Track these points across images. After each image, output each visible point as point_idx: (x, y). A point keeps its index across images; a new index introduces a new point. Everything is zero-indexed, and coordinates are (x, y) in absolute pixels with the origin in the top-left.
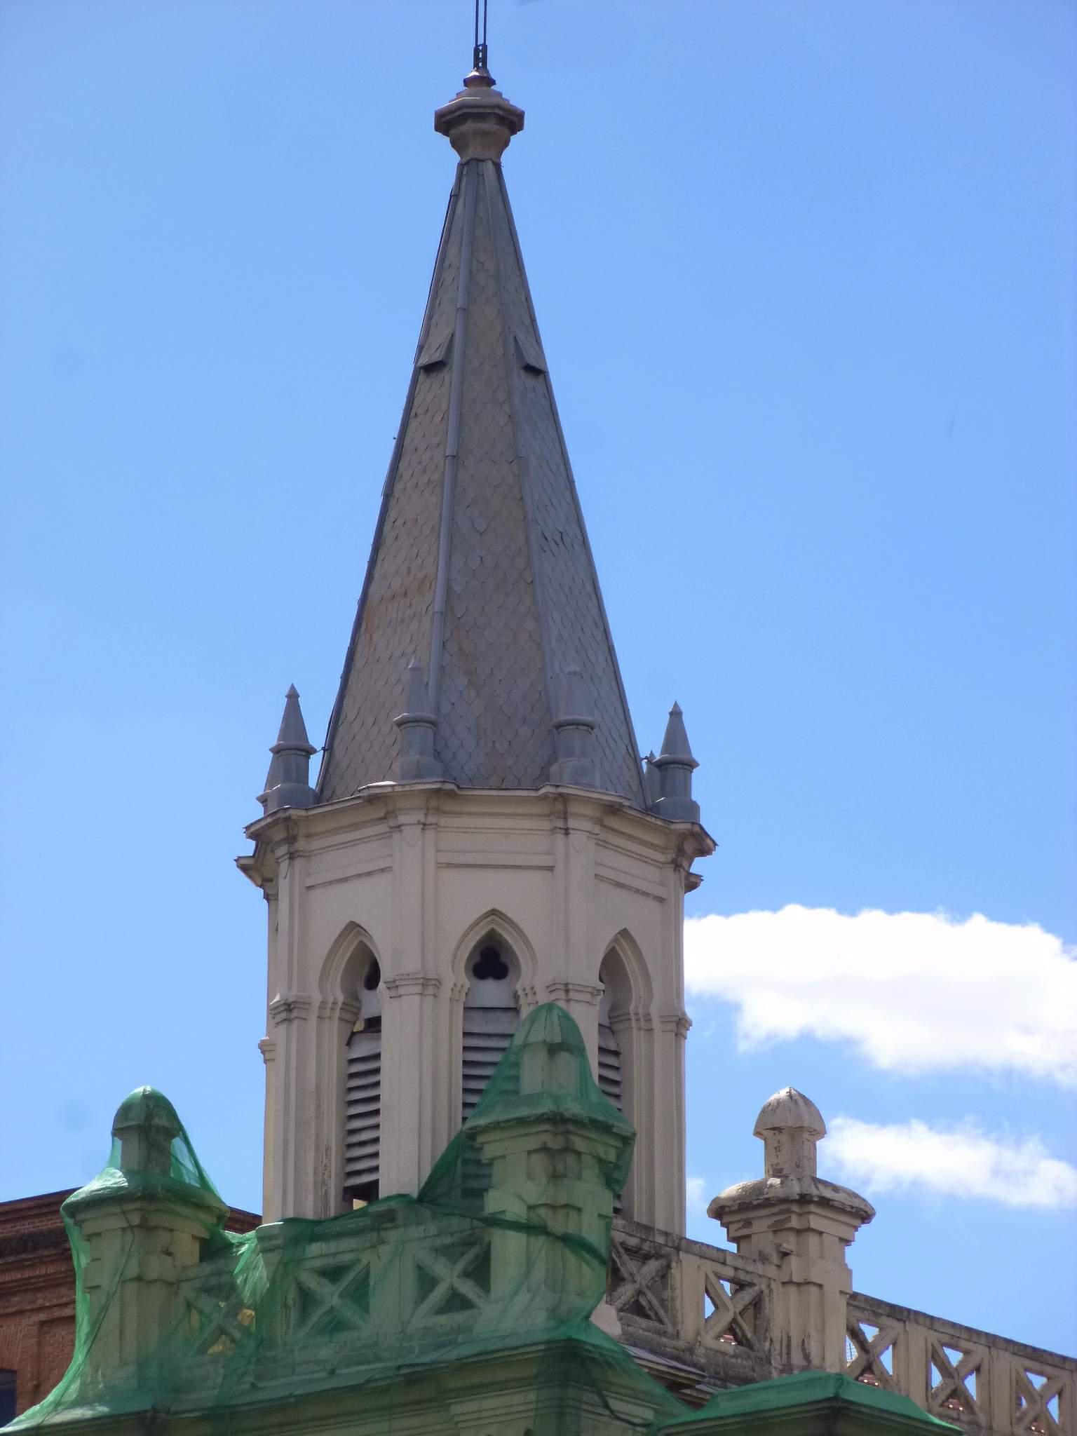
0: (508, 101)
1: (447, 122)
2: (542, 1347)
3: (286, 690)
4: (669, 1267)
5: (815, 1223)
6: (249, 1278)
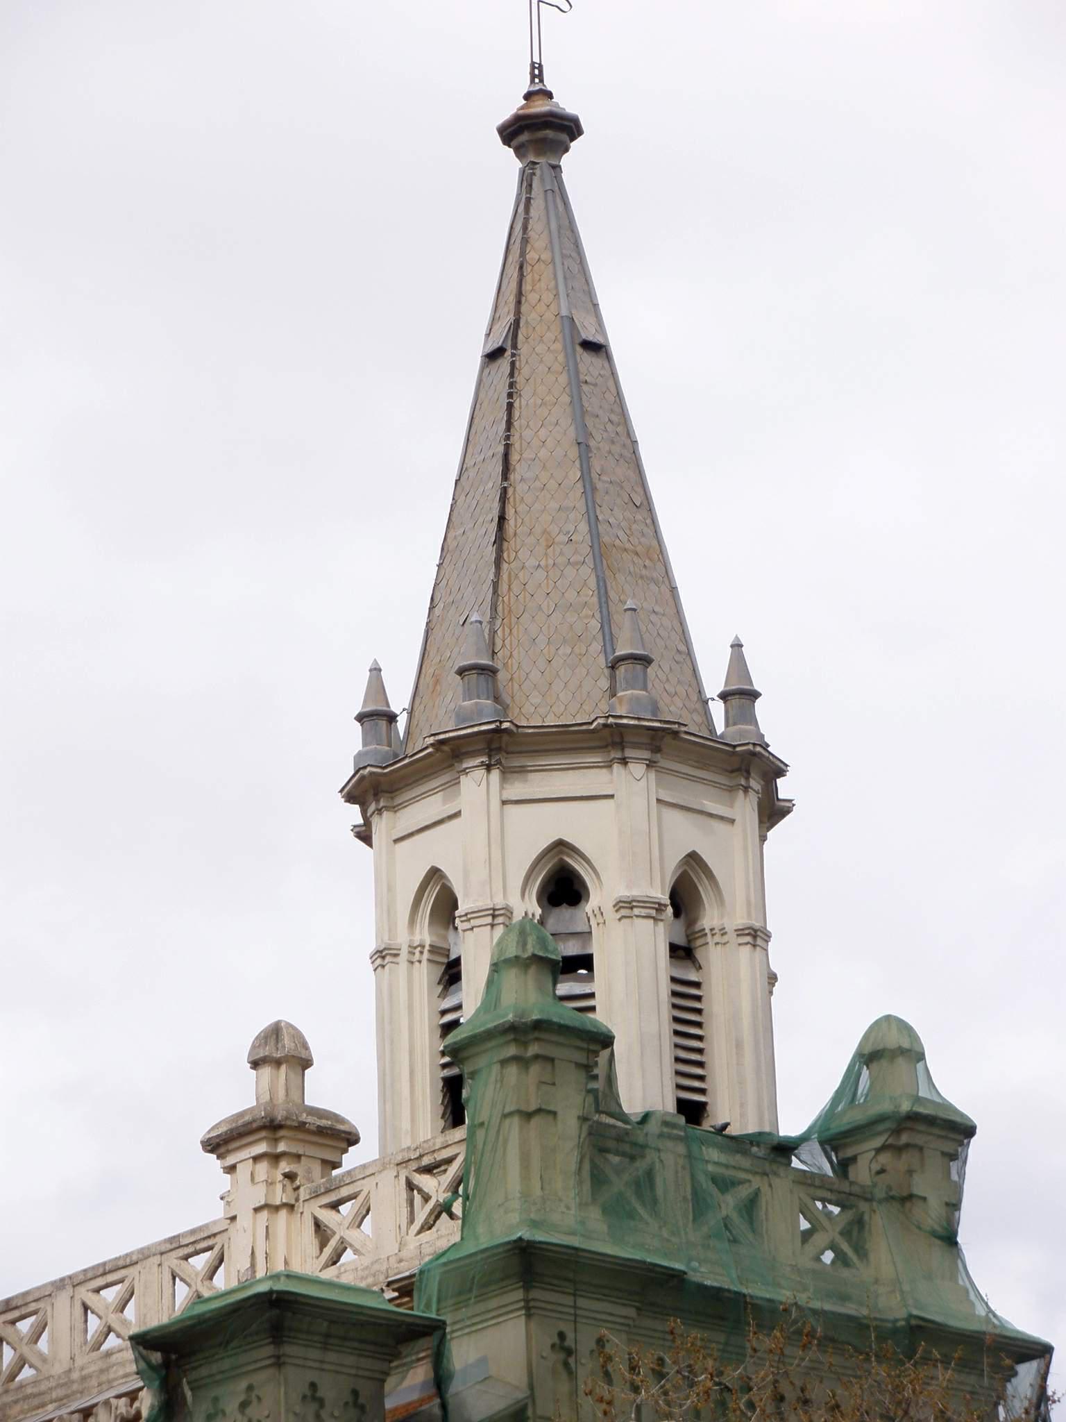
0: (564, 109)
1: (512, 132)
2: (501, 1250)
3: (369, 666)
5: (919, 1139)
6: (415, 709)
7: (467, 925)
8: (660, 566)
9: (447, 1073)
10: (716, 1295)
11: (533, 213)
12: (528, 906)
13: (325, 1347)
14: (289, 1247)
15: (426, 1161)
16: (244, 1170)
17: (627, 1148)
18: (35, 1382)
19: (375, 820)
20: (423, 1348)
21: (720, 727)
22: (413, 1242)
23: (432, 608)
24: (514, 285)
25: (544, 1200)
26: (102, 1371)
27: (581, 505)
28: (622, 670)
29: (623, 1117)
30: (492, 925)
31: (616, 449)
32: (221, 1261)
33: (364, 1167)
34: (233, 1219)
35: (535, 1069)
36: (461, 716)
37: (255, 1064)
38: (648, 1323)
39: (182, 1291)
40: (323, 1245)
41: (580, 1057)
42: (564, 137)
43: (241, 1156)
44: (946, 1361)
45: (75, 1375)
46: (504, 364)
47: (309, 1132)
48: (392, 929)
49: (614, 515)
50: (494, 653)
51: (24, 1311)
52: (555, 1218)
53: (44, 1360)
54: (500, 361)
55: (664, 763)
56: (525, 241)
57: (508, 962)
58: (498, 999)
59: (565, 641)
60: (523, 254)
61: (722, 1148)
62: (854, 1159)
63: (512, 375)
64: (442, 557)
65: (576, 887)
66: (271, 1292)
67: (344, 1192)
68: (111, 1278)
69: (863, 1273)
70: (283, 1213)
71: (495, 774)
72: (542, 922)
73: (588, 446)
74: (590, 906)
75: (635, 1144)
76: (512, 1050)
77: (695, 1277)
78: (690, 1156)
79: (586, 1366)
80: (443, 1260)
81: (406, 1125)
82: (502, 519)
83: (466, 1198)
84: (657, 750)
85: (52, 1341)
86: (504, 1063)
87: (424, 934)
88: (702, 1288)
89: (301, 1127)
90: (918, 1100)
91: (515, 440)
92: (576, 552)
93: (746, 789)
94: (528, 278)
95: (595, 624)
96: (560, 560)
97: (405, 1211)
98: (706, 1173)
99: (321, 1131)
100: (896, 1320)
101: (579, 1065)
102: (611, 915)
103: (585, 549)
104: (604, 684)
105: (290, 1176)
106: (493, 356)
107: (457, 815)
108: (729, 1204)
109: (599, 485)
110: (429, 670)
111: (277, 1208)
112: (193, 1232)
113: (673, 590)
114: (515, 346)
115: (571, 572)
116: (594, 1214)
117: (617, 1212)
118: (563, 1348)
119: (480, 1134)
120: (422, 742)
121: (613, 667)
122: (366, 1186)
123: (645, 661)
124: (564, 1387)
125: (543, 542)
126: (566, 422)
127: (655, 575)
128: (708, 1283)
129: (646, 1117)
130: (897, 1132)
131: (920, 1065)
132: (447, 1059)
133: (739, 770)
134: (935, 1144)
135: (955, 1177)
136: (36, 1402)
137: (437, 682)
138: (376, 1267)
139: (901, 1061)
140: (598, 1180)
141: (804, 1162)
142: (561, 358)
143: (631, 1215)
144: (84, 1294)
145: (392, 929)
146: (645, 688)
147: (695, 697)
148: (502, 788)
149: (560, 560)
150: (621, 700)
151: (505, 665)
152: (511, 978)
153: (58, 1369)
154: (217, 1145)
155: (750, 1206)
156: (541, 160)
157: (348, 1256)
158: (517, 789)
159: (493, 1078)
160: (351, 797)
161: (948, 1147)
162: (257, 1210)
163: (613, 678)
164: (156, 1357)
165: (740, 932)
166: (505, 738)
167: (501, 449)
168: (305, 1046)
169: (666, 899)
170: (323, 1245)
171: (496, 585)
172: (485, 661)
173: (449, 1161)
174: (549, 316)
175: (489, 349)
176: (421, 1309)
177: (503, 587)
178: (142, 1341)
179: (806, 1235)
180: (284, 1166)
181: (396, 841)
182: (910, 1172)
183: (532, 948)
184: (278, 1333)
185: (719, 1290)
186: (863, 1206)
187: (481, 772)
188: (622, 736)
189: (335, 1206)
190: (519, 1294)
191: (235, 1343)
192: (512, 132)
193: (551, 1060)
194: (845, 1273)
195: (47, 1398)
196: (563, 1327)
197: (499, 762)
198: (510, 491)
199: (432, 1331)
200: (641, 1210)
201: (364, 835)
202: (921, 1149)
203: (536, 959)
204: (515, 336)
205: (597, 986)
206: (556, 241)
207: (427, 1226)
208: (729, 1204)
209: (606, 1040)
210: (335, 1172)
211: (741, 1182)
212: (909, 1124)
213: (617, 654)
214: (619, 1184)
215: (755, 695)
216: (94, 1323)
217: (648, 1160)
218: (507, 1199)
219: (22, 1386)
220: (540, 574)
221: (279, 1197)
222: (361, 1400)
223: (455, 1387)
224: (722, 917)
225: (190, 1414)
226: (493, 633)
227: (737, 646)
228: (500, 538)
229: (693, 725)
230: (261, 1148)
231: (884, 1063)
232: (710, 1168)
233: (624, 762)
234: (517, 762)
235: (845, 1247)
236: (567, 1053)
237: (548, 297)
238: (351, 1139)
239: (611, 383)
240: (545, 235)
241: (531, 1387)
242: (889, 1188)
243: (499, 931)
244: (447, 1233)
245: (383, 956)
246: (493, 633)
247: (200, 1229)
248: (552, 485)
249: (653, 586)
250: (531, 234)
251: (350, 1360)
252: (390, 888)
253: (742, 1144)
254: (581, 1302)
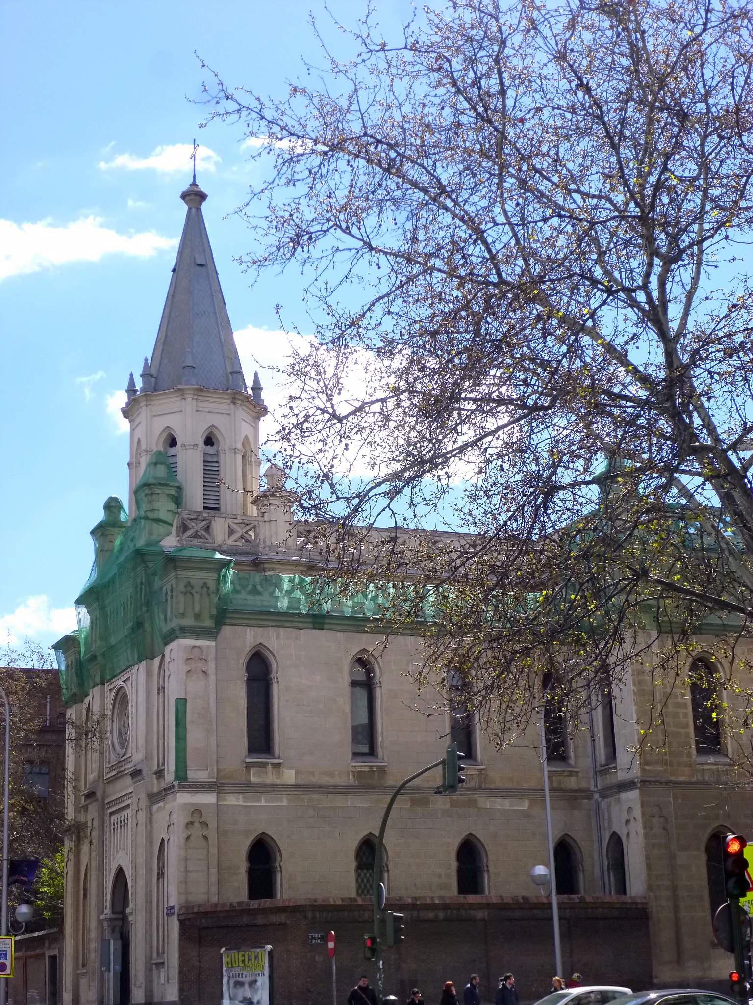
4: (210, 522)
192: (184, 196)
233: (185, 399)
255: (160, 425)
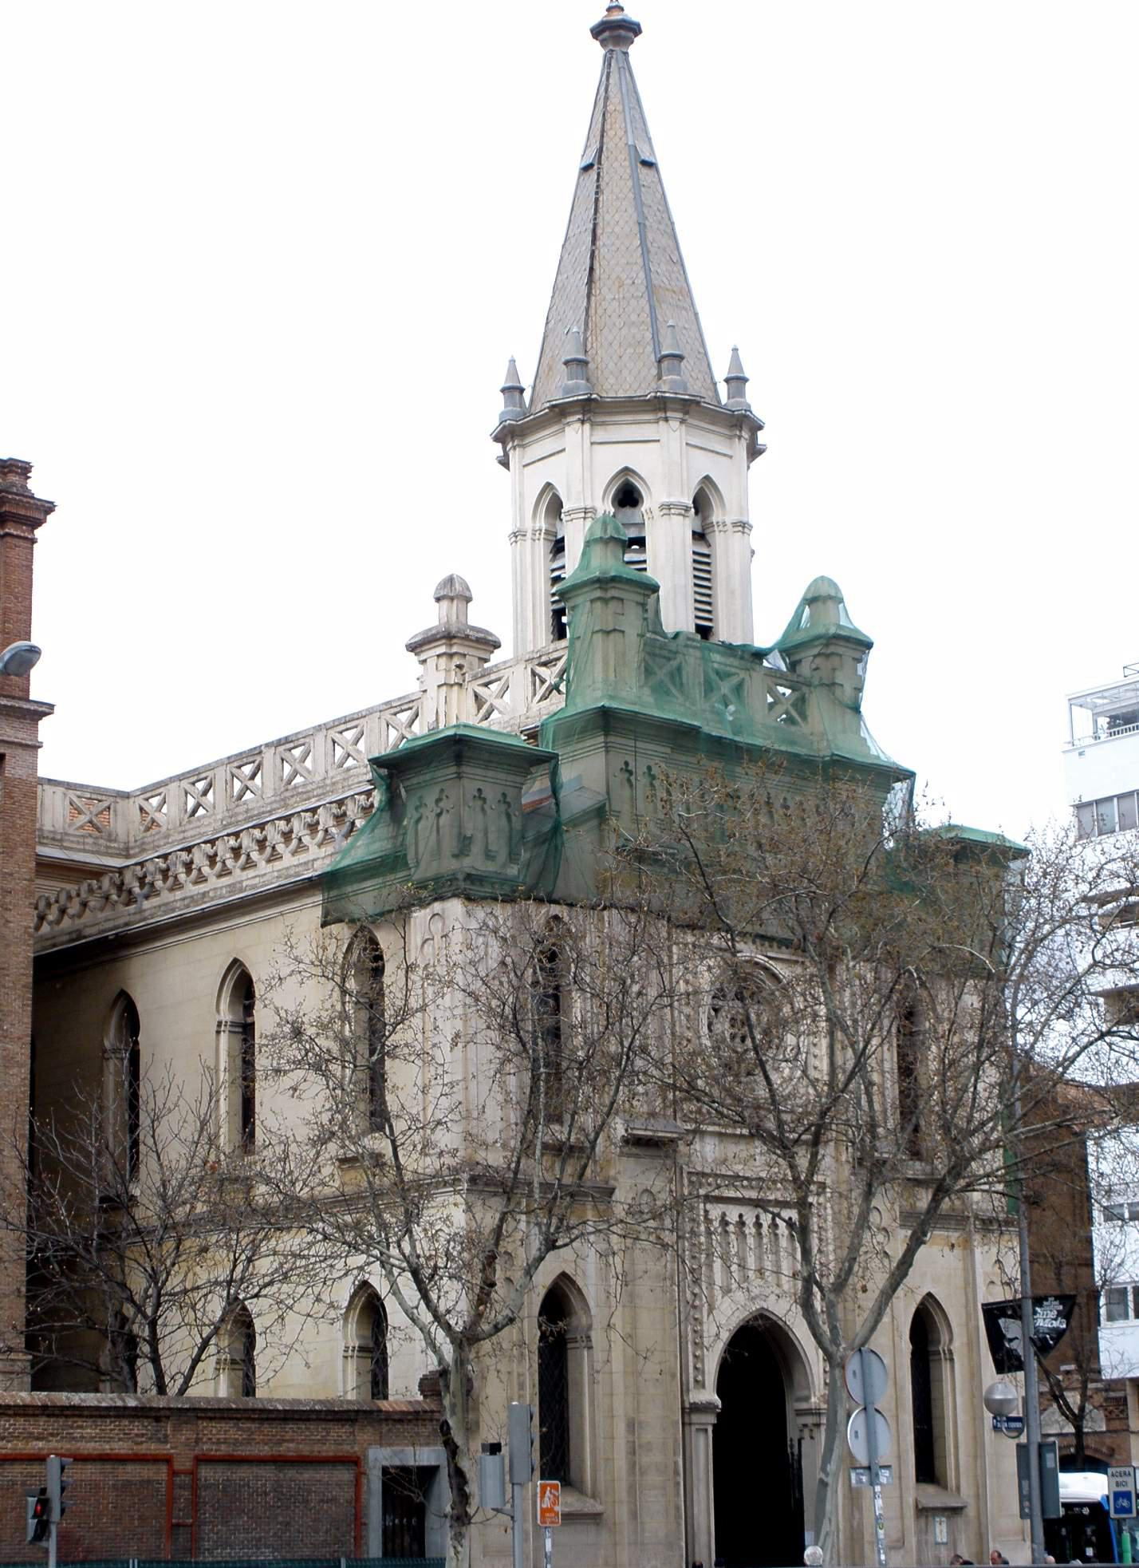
1: (598, 32)
5: (840, 650)
7: (569, 518)
8: (688, 300)
9: (555, 607)
10: (719, 741)
11: (611, 81)
12: (606, 507)
13: (487, 768)
14: (459, 709)
15: (543, 659)
16: (431, 663)
17: (665, 653)
18: (304, 785)
19: (511, 454)
20: (545, 769)
21: (724, 399)
22: (535, 706)
23: (547, 323)
24: (599, 126)
25: (616, 682)
26: (344, 779)
27: (640, 261)
28: (665, 364)
29: (664, 635)
30: (585, 518)
31: (662, 227)
32: (417, 716)
33: (505, 662)
34: (425, 691)
35: (612, 605)
36: (568, 391)
37: (438, 600)
38: (676, 756)
39: (393, 734)
40: (479, 709)
41: (640, 599)
42: (631, 35)
43: (430, 654)
44: (864, 782)
45: (328, 782)
46: (593, 174)
47: (472, 641)
48: (522, 519)
49: (659, 267)
50: (586, 351)
51: (296, 743)
52: (624, 694)
53: (309, 772)
54: (590, 171)
55: (690, 421)
56: (606, 98)
57: (596, 541)
58: (589, 562)
59: (630, 345)
60: (605, 106)
61: (723, 654)
62: (800, 661)
63: (598, 180)
64: (554, 293)
65: (635, 495)
66: (455, 735)
67: (493, 677)
68: (349, 725)
69: (804, 728)
70: (456, 688)
71: (587, 426)
72: (614, 516)
73: (645, 225)
74: (645, 507)
75: (670, 651)
76: (598, 594)
77: (706, 729)
78: (703, 658)
79: (642, 781)
80: (556, 717)
81: (530, 636)
82: (592, 269)
83: (568, 681)
84: (686, 413)
85: (314, 761)
86: (592, 601)
87: (542, 523)
88: (710, 736)
89: (467, 638)
90: (839, 627)
91: (600, 220)
92: (637, 290)
93: (740, 437)
94: (608, 121)
95: (649, 335)
96: (628, 295)
97: (530, 688)
98: (713, 668)
99: (478, 640)
100: (824, 757)
101: (638, 603)
102: (657, 513)
103: (643, 288)
104: (654, 371)
105: (460, 667)
106: (587, 168)
107: (563, 450)
108: (725, 688)
109: (652, 249)
110: (545, 361)
111: (452, 685)
112: (400, 699)
113: (696, 314)
114: (600, 163)
115: (633, 302)
116: (647, 691)
117: (660, 690)
118: (627, 770)
119: (578, 644)
120: (542, 407)
121: (660, 362)
122: (505, 673)
123: (680, 358)
124: (627, 792)
125: (617, 284)
126: (631, 210)
127: (685, 305)
128: (714, 734)
129: (677, 635)
130: (827, 645)
131: (841, 606)
132: (556, 598)
133: (736, 425)
134: (848, 652)
135: (860, 672)
136: (305, 796)
137: (550, 369)
138: (512, 722)
139: (830, 604)
140: (648, 672)
141: (776, 662)
142: (628, 171)
143: (668, 693)
144: (333, 734)
145: (522, 519)
146: (679, 375)
147: (709, 381)
148: (591, 435)
149: (628, 295)
150: (665, 382)
151: (593, 359)
152: (597, 551)
153: (318, 778)
154: (414, 648)
155: (739, 688)
156: (617, 49)
157: (495, 715)
158: (601, 434)
159: (587, 610)
160: (497, 439)
161: (857, 655)
162: (439, 686)
163: (659, 368)
164: (384, 772)
165: (735, 525)
166: (593, 404)
167: (591, 226)
168: (468, 589)
169: (690, 503)
170: (479, 709)
171: (587, 310)
172: (581, 356)
173: (558, 659)
174: (621, 144)
175: (584, 164)
176: (546, 747)
177: (592, 311)
178: (376, 762)
179: (771, 706)
180: (457, 661)
181: (525, 466)
182: (834, 670)
183: (610, 532)
184: (459, 759)
185: (721, 738)
186: (805, 689)
187: (578, 425)
188: (665, 403)
189: (486, 685)
190: (602, 739)
191: (433, 765)
192: (598, 32)
193: (622, 600)
194: (793, 729)
195: (311, 794)
196: (628, 758)
197: (589, 419)
198: (597, 252)
199: (549, 760)
200: (674, 691)
201: (505, 462)
202: (841, 655)
203: (612, 538)
204: (600, 157)
205: (648, 555)
206: (625, 97)
207: (544, 698)
208: (725, 688)
209: (655, 589)
210: (486, 665)
211: (734, 674)
212: (834, 641)
213: (663, 353)
214: (661, 674)
215: (745, 380)
216: (339, 752)
217: (678, 660)
218: (594, 682)
219: (295, 787)
220: (615, 304)
221: (453, 679)
222: (508, 800)
223: (562, 794)
224: (724, 515)
225: (404, 805)
226: (586, 339)
227: (735, 350)
228: (590, 281)
229: (708, 397)
230: (443, 649)
231: (820, 604)
232: (716, 665)
233: (666, 420)
234: (599, 419)
235: (794, 714)
236: (631, 596)
237: (621, 133)
238: (496, 645)
239: (659, 187)
240: (619, 96)
241: (608, 793)
242: (821, 679)
243: (589, 522)
244: (557, 702)
245: (517, 535)
246: (586, 339)
247: (404, 697)
248: (623, 248)
249: (684, 312)
250: (610, 94)
251: (502, 776)
252: (521, 495)
253: (729, 649)
254: (639, 744)
255: (610, 461)
